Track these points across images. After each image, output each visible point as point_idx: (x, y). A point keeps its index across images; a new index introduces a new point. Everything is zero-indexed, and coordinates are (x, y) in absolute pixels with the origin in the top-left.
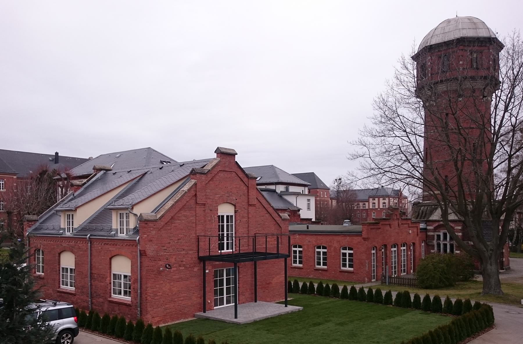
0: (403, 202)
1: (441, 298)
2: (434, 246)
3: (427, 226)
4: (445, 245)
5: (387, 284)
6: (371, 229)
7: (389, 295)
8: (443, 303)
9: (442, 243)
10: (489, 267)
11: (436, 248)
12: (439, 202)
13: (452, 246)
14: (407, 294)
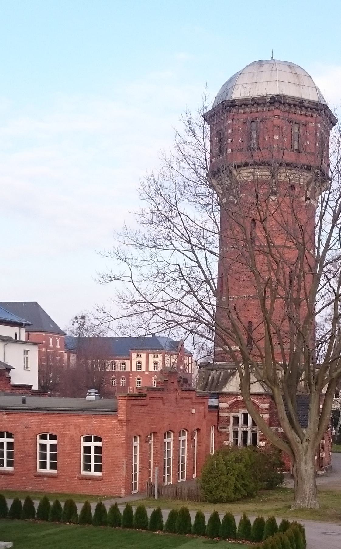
2: (228, 434)
3: (219, 402)
4: (245, 433)
5: (156, 497)
6: (133, 405)
7: (157, 515)
8: (237, 525)
9: (240, 430)
10: (303, 466)
13: (254, 435)
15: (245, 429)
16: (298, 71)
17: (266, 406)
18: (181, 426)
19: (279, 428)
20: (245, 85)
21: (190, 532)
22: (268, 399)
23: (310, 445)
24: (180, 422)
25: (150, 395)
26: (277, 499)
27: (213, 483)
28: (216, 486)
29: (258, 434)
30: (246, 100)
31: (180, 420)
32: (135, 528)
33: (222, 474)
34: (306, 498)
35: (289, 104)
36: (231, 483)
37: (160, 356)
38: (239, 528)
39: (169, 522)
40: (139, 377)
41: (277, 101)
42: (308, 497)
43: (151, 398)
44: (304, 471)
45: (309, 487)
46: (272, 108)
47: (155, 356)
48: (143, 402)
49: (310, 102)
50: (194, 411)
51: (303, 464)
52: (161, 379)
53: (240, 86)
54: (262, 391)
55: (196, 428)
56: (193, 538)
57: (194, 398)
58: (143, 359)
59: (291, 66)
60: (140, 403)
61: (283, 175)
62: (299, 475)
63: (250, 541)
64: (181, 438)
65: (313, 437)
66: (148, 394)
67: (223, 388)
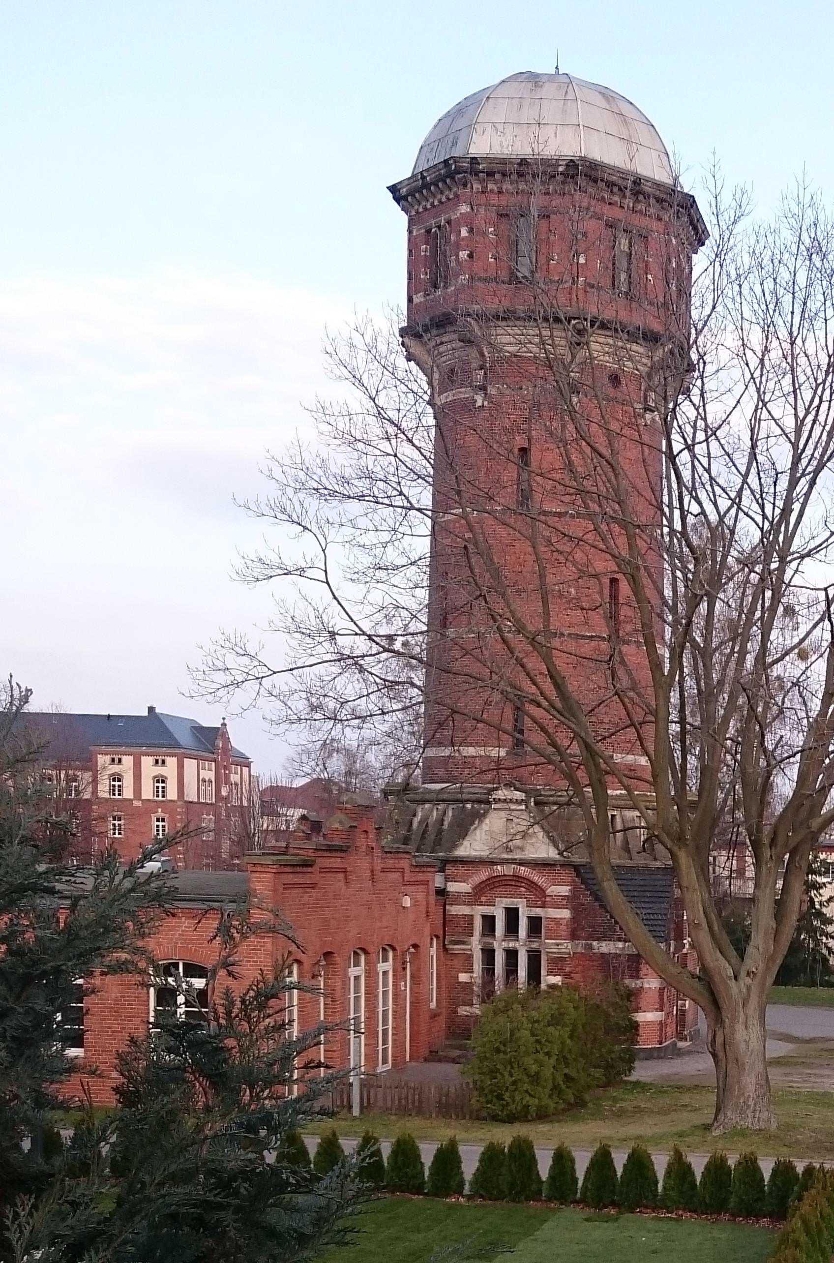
0: (235, 778)
1: (575, 1154)
2: (470, 956)
3: (447, 879)
4: (512, 955)
5: (356, 1111)
6: (287, 886)
7: (448, 1158)
8: (661, 1174)
9: (500, 947)
10: (740, 1034)
11: (478, 965)
12: (579, 792)
13: (534, 959)
14: (523, 1153)
15: (511, 945)
16: (625, 109)
17: (564, 890)
18: (382, 939)
19: (595, 943)
20: (500, 127)
21: (536, 1196)
22: (568, 875)
23: (755, 984)
24: (380, 928)
25: (321, 863)
26: (638, 1110)
27: (506, 1074)
28: (514, 1083)
29: (544, 957)
30: (504, 161)
31: (379, 924)
32: (393, 1192)
33: (527, 1053)
34: (749, 1107)
35: (610, 185)
36: (547, 1072)
37: (172, 762)
38: (665, 1182)
39: (480, 1173)
40: (160, 814)
41: (582, 173)
42: (751, 1102)
43: (324, 870)
44: (743, 1046)
45: (754, 1081)
46: (569, 187)
47: (157, 762)
48: (306, 879)
49: (658, 185)
50: (407, 902)
51: (740, 1027)
52: (340, 822)
53: (489, 127)
54: (552, 854)
55: (411, 942)
56: (553, 1210)
57: (407, 871)
58: (170, 769)
59: (607, 94)
60: (302, 881)
61: (600, 346)
62: (729, 1055)
63: (695, 1211)
64: (382, 967)
65: (762, 966)
66: (318, 860)
67: (457, 846)
